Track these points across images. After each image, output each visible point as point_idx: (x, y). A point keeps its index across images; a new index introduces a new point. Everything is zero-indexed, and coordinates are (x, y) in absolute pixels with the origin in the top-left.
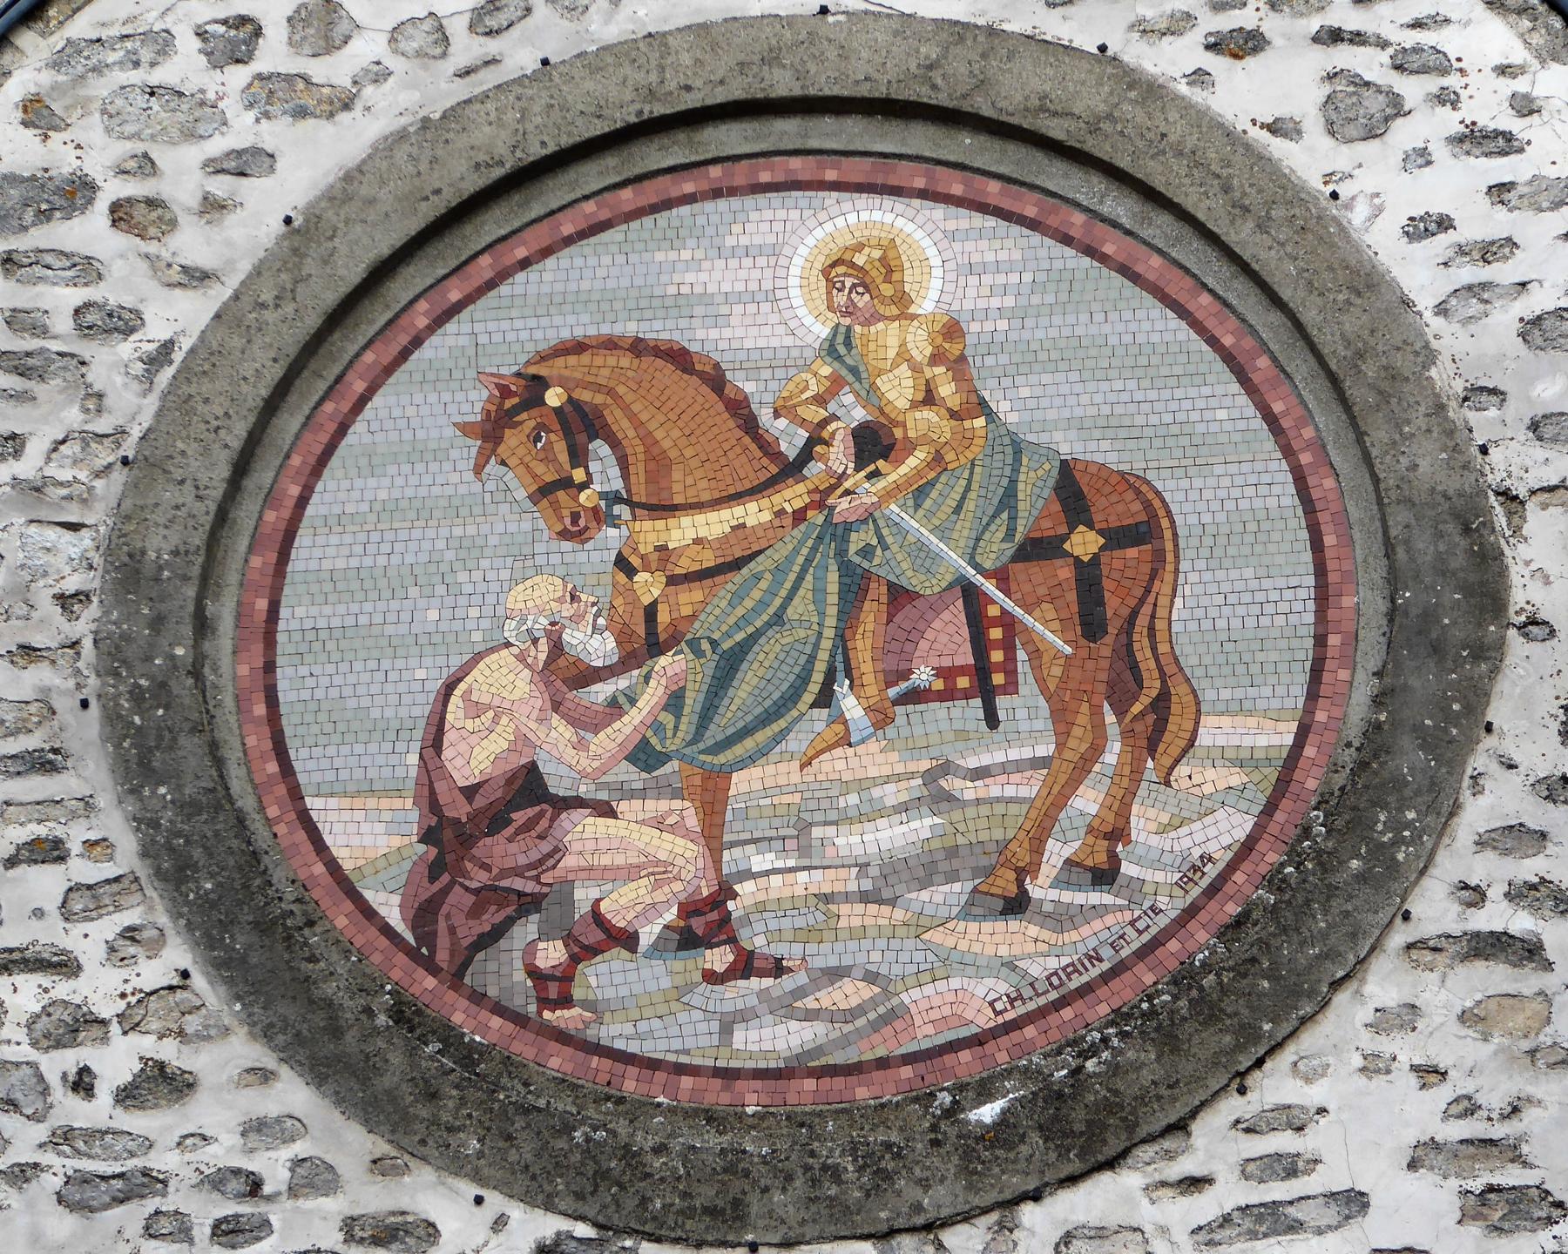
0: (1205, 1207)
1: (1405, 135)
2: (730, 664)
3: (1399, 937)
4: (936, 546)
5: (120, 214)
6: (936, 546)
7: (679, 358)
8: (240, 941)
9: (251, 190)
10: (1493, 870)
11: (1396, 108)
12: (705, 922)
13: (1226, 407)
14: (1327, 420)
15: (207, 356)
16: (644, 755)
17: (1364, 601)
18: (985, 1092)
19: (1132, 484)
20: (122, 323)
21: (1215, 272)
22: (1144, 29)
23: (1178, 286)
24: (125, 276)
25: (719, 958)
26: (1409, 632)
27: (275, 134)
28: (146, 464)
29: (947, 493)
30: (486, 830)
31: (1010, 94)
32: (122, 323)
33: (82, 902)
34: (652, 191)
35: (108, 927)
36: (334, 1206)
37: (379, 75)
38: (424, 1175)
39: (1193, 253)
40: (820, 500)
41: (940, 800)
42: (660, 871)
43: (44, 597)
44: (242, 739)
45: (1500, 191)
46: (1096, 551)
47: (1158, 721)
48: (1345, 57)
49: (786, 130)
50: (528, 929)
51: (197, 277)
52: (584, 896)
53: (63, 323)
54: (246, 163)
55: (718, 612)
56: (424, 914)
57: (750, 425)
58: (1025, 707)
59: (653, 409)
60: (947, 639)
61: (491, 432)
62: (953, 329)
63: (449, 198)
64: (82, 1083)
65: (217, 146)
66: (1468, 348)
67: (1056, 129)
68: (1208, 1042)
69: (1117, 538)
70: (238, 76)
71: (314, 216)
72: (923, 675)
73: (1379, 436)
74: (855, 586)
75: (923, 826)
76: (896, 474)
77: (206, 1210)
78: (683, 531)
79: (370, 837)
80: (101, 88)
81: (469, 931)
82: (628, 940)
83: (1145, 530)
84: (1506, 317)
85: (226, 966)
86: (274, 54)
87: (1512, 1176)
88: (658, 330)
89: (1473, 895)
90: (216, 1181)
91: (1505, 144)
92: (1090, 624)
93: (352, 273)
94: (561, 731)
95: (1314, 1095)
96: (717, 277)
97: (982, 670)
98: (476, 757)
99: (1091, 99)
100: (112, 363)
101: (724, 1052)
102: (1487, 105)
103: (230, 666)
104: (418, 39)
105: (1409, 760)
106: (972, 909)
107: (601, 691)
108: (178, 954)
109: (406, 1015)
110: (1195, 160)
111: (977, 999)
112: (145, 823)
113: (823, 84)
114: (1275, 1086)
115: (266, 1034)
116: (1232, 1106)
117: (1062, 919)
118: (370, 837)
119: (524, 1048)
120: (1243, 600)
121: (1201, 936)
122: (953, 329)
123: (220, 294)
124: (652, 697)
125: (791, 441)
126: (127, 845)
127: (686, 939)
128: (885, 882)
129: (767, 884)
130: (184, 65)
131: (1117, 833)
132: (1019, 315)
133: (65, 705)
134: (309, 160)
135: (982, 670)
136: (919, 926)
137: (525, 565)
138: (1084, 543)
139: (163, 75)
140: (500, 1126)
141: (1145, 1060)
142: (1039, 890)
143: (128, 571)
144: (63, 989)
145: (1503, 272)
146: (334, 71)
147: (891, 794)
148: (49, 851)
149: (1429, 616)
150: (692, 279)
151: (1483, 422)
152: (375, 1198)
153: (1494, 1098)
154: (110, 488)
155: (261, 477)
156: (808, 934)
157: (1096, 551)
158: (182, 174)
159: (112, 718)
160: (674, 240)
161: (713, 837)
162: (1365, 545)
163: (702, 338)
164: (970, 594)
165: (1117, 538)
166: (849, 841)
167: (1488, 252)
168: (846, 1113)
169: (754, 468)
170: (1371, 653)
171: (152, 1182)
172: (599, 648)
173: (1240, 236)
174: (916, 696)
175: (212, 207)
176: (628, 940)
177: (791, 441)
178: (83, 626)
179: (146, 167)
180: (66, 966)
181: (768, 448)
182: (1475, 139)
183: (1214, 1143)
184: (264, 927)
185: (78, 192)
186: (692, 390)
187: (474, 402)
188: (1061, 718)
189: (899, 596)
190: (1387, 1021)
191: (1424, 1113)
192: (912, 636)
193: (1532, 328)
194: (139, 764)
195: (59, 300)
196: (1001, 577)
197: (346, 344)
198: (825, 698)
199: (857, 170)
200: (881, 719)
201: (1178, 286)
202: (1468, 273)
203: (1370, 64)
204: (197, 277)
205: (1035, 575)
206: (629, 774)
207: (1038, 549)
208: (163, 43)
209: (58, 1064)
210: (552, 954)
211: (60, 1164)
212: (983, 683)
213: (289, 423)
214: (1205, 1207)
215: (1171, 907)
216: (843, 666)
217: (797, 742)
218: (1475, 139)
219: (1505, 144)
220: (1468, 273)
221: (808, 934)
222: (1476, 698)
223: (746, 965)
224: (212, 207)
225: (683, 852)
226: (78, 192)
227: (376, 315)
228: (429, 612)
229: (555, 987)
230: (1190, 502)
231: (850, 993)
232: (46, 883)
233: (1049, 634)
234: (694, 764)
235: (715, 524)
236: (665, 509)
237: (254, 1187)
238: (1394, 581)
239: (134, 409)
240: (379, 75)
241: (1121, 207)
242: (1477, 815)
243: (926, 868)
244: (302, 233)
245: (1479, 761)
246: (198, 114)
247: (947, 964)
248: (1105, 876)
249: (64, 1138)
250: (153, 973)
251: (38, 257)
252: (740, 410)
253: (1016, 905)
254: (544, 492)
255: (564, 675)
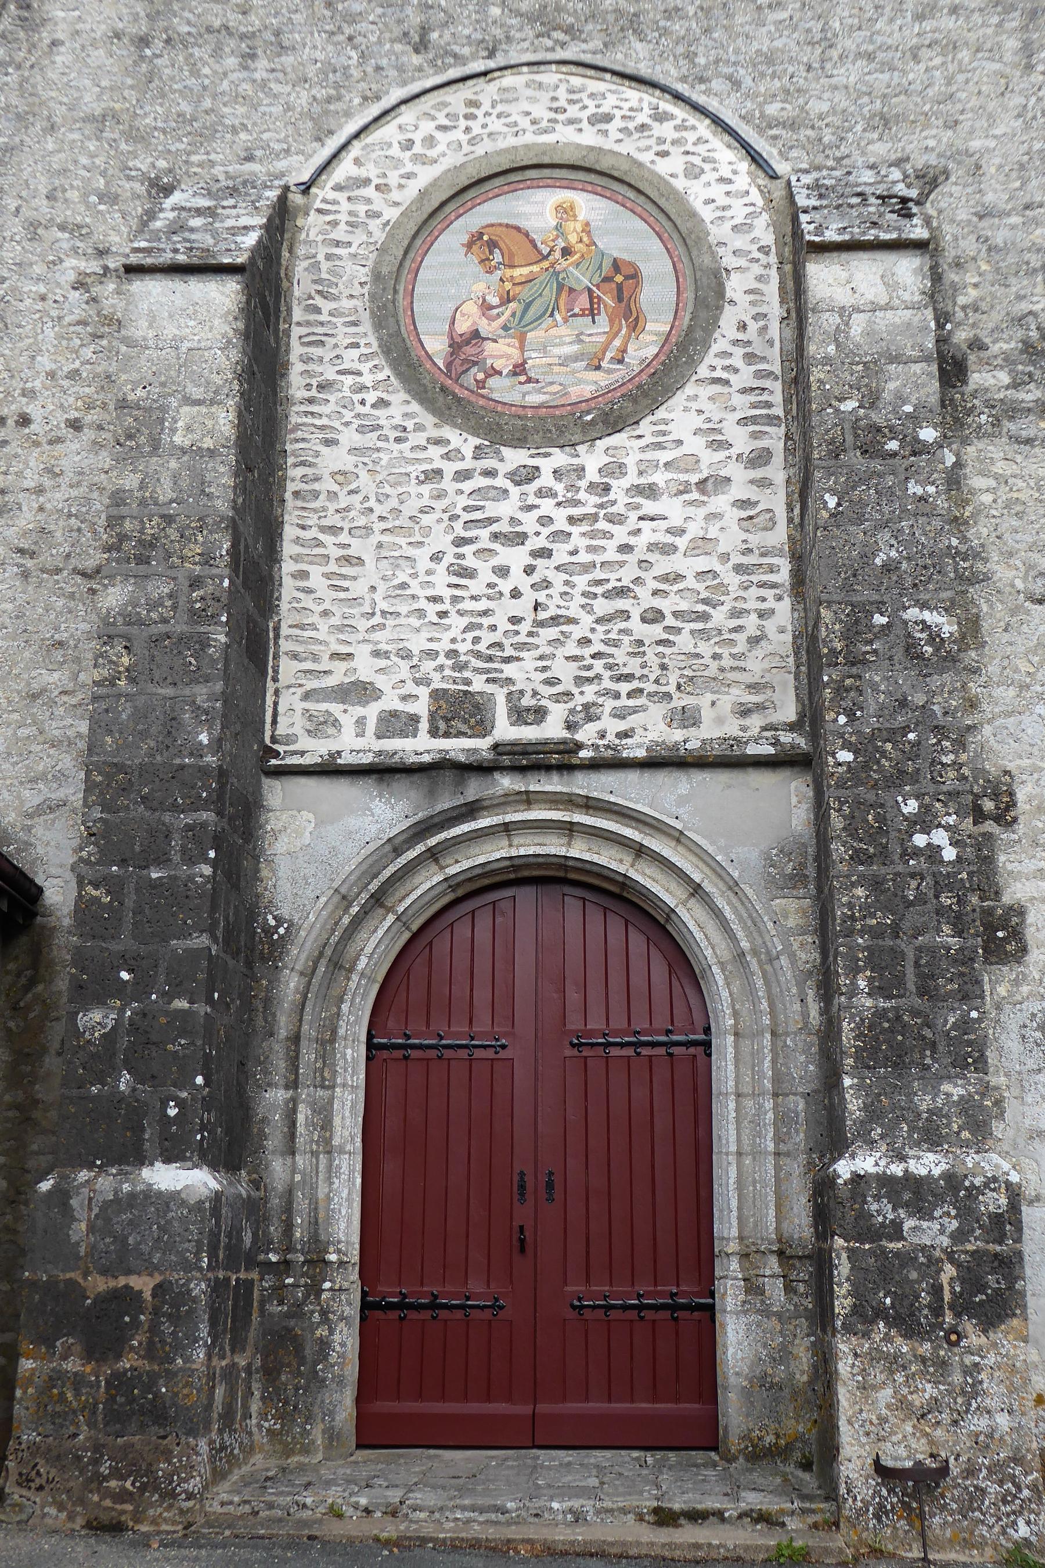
0: (642, 442)
1: (704, 178)
2: (528, 306)
3: (694, 378)
4: (581, 278)
5: (378, 188)
6: (581, 278)
7: (518, 229)
8: (403, 369)
9: (411, 183)
10: (719, 363)
11: (703, 171)
12: (519, 369)
13: (657, 246)
14: (681, 249)
15: (398, 224)
16: (505, 328)
17: (689, 295)
18: (588, 413)
19: (631, 264)
20: (377, 215)
21: (655, 211)
22: (639, 150)
23: (645, 215)
24: (378, 202)
25: (523, 378)
26: (700, 302)
27: (417, 168)
28: (382, 250)
29: (584, 265)
30: (465, 345)
31: (604, 165)
32: (377, 215)
33: (364, 358)
34: (512, 187)
35: (370, 364)
36: (424, 435)
37: (444, 155)
38: (447, 428)
39: (649, 207)
40: (552, 265)
41: (581, 341)
42: (508, 357)
43: (356, 283)
44: (405, 321)
45: (728, 193)
46: (622, 280)
47: (636, 325)
48: (690, 158)
49: (547, 172)
50: (475, 369)
51: (396, 204)
52: (489, 362)
53: (362, 214)
54: (409, 176)
55: (525, 293)
56: (449, 365)
57: (535, 246)
58: (602, 319)
59: (508, 240)
60: (583, 301)
61: (469, 245)
62: (587, 224)
63: (461, 186)
64: (363, 402)
65: (402, 171)
66: (717, 232)
67: (616, 174)
68: (646, 402)
69: (627, 277)
70: (408, 154)
71: (426, 190)
72: (577, 310)
73: (694, 253)
74: (560, 287)
75: (575, 348)
76: (571, 260)
77: (393, 435)
78: (517, 272)
79: (436, 346)
80: (374, 156)
81: (460, 370)
82: (500, 373)
83: (635, 276)
84: (728, 225)
85: (399, 375)
86: (418, 148)
87: (719, 437)
88: (511, 222)
89: (713, 368)
90: (395, 428)
91: (730, 181)
92: (620, 299)
93: (436, 205)
94: (485, 321)
95: (670, 416)
96: (527, 209)
97: (592, 309)
98: (463, 327)
99: (625, 166)
100: (374, 225)
101: (349, 1147)
102: (725, 172)
103: (402, 302)
104: (455, 146)
105: (698, 334)
106: (587, 368)
107: (495, 312)
108: (387, 372)
109: (444, 389)
110: (651, 183)
111: (587, 391)
112: (380, 339)
113: (557, 160)
114: (661, 413)
115: (409, 392)
116: (650, 418)
117: (609, 372)
118: (436, 346)
119: (473, 398)
120: (659, 295)
121: (644, 377)
122: (587, 224)
123: (402, 209)
124: (508, 313)
125: (545, 252)
126: (375, 344)
127: (514, 374)
128: (565, 361)
129: (535, 361)
130: (395, 151)
131: (625, 351)
132: (605, 221)
133: (361, 310)
134: (426, 175)
135: (592, 309)
136: (574, 372)
137: (477, 279)
138: (619, 278)
139: (389, 153)
140: (466, 418)
141: (629, 406)
142: (604, 364)
143: (377, 276)
144: (358, 379)
145: (728, 214)
146: (432, 153)
147: (568, 339)
148: (356, 345)
149: (705, 298)
150: (522, 209)
151: (721, 251)
152: (435, 433)
153: (716, 419)
154: (373, 256)
155: (411, 255)
156: (544, 373)
157: (622, 280)
158: (393, 178)
159: (372, 312)
160: (518, 199)
161: (522, 348)
162: (690, 281)
163: (523, 224)
164: (590, 290)
165: (627, 277)
166: (557, 351)
167: (724, 209)
168: (553, 417)
169: (536, 257)
170: (690, 308)
171: (379, 427)
172: (495, 301)
173: (662, 202)
174: (575, 315)
175: (401, 186)
176: (500, 373)
177: (545, 252)
178: (366, 290)
179: (385, 175)
180: (359, 374)
181: (540, 252)
182: (722, 180)
183: (645, 427)
184: (409, 366)
185: (367, 182)
186: (521, 237)
187: (465, 238)
188: (611, 322)
189: (571, 290)
190: (689, 399)
191: (698, 422)
192: (574, 301)
193: (734, 228)
194: (379, 324)
195: (362, 209)
196: (598, 286)
197: (434, 222)
198: (552, 315)
199: (565, 183)
200: (566, 320)
201: (645, 215)
202: (719, 214)
203: (697, 160)
204: (396, 204)
205: (606, 286)
206: (502, 332)
207: (607, 279)
208: (390, 145)
209: (357, 397)
210: (481, 376)
211: (357, 422)
212: (592, 313)
213: (418, 242)
214: (642, 442)
215: (637, 370)
216: (557, 307)
217: (544, 326)
218: (722, 180)
219: (730, 181)
220: (719, 214)
221: (544, 373)
222: (716, 319)
223: (529, 380)
224: (401, 186)
225: (515, 352)
226: (367, 182)
227: (441, 216)
228: (451, 290)
229: (481, 384)
230: (646, 269)
231: (555, 388)
232: (355, 353)
233: (609, 301)
234: (517, 331)
235: (525, 271)
236: (512, 266)
237: (405, 429)
238: (696, 290)
239: (379, 236)
240: (444, 155)
241: (631, 194)
242: (715, 348)
243: (576, 358)
244: (423, 194)
245: (716, 335)
246: (398, 163)
247: (580, 382)
248: (621, 361)
249: (358, 416)
250: (381, 376)
251: (357, 198)
252: (533, 242)
253: (598, 368)
254: (482, 261)
255: (486, 307)
